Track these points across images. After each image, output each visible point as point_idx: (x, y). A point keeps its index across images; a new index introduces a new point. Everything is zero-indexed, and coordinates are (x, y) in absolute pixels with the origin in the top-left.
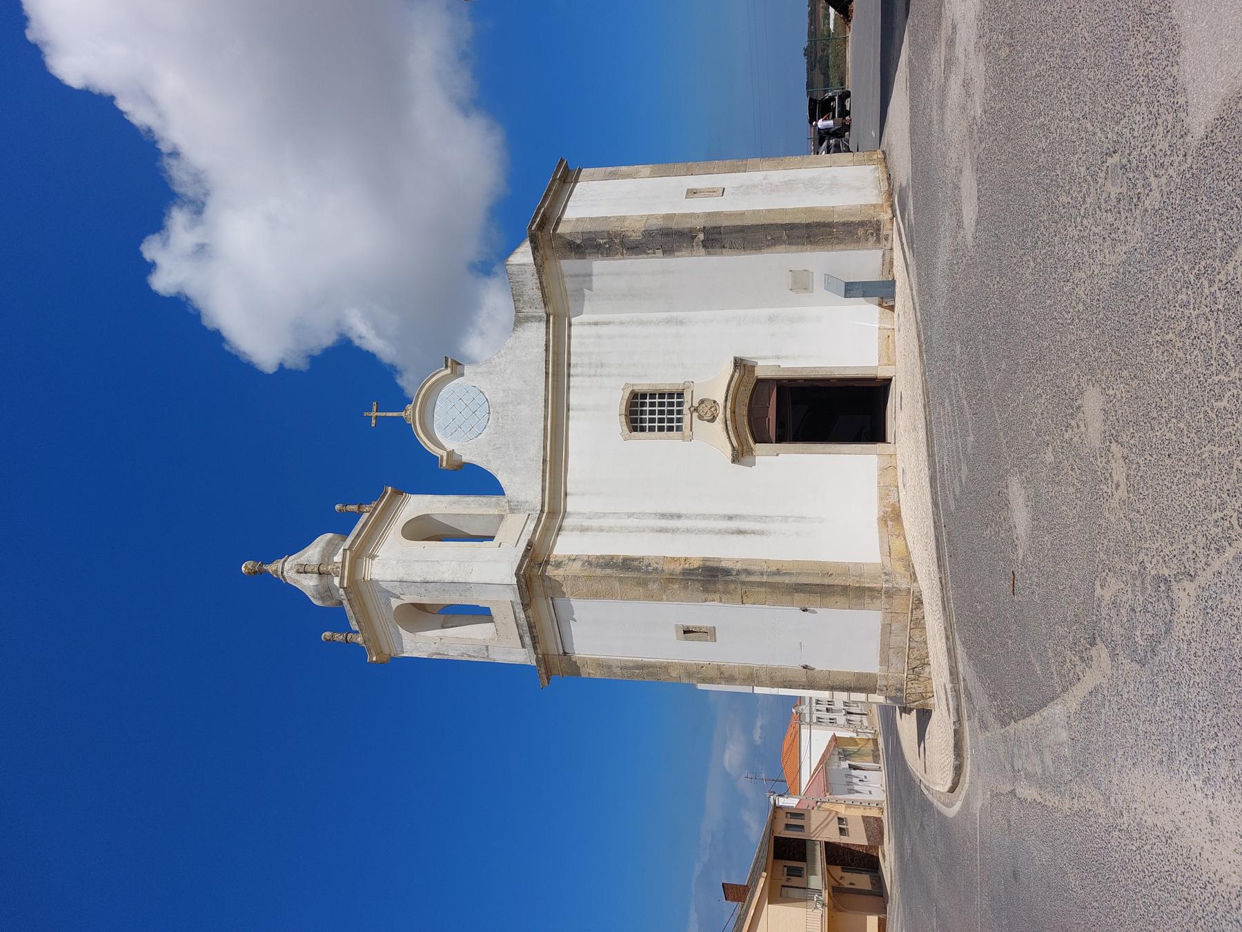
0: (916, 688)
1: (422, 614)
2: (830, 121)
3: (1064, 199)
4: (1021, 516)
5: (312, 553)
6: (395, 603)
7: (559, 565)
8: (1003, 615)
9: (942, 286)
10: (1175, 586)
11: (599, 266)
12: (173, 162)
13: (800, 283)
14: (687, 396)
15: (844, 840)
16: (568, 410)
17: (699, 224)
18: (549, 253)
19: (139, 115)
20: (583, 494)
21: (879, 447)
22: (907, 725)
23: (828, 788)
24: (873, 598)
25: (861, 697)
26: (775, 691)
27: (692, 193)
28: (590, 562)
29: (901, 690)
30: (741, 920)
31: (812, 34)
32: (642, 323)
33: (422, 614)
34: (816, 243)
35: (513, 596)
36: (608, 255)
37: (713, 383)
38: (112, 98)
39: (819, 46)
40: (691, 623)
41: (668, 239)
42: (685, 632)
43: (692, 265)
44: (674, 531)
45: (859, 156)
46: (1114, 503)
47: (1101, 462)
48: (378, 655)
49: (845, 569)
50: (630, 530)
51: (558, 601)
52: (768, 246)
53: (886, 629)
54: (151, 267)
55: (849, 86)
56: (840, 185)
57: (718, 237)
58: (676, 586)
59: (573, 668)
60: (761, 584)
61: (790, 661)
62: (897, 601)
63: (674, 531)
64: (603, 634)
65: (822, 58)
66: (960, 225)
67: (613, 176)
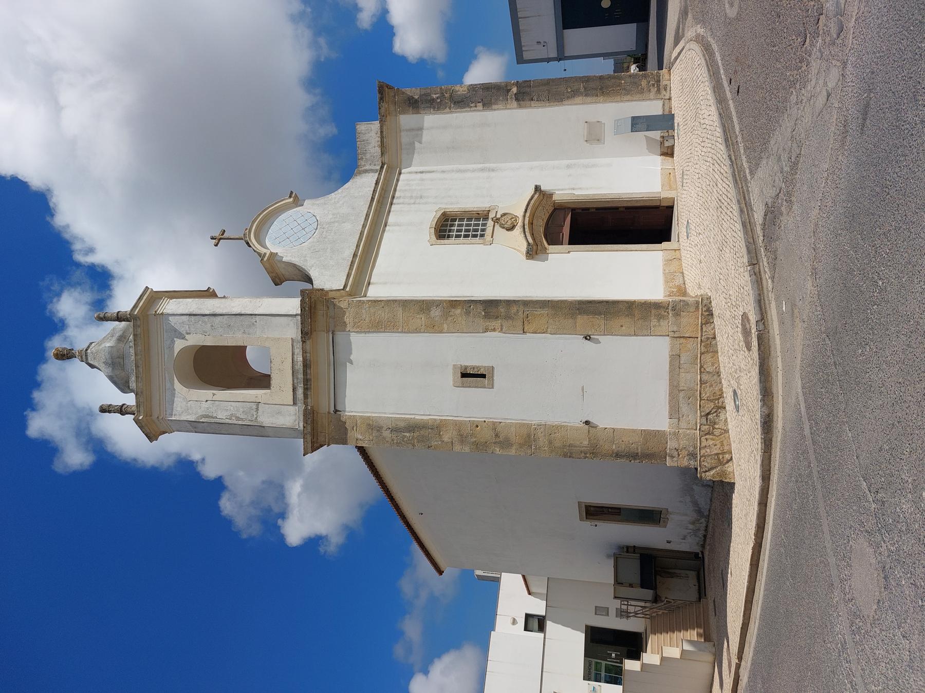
6: (179, 345)
11: (430, 120)
13: (594, 135)
16: (386, 225)
18: (392, 108)
20: (385, 283)
21: (665, 245)
24: (660, 317)
29: (693, 455)
32: (460, 171)
34: (608, 94)
36: (439, 109)
37: (515, 201)
40: (473, 361)
42: (464, 375)
48: (146, 416)
51: (340, 336)
52: (568, 98)
53: (675, 358)
58: (458, 311)
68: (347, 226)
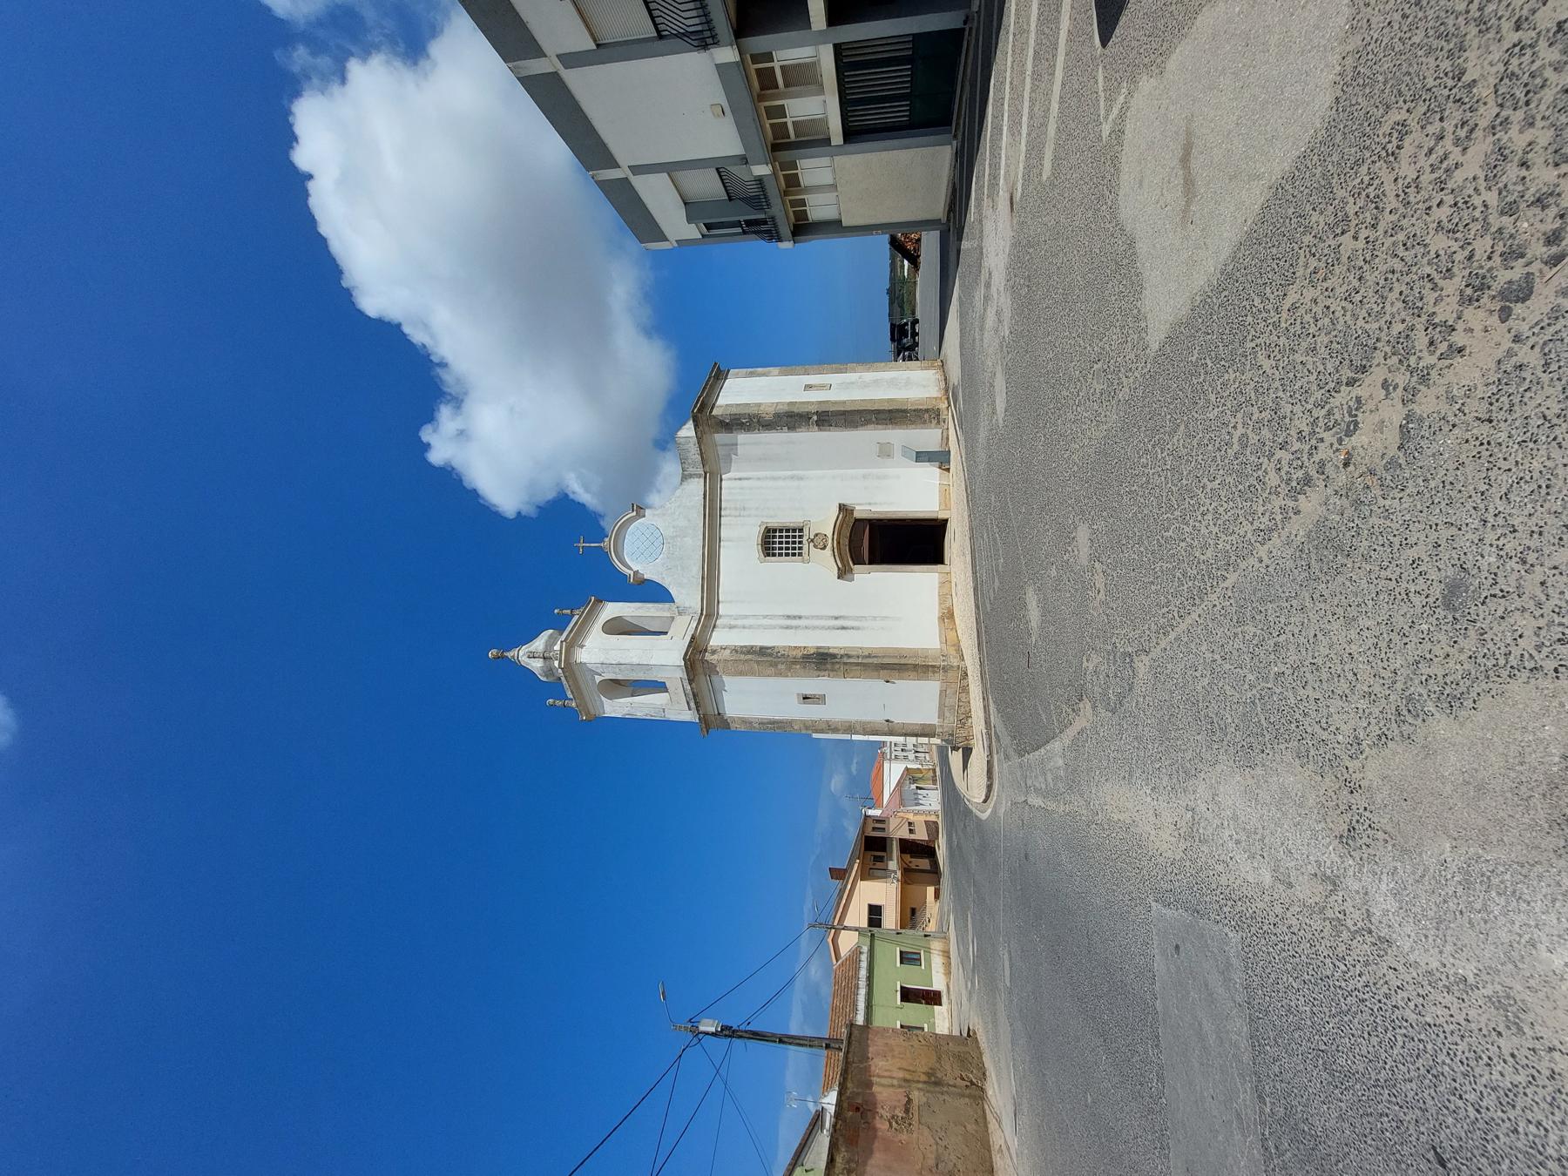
0: (963, 733)
1: (617, 687)
2: (904, 342)
3: (1065, 393)
4: (1034, 615)
5: (539, 644)
6: (598, 679)
7: (714, 652)
8: (1022, 680)
9: (982, 455)
10: (1136, 659)
11: (742, 438)
12: (439, 370)
13: (885, 452)
14: (806, 531)
15: (912, 837)
17: (813, 409)
19: (417, 336)
21: (939, 567)
22: (956, 758)
23: (902, 803)
25: (925, 740)
26: (866, 738)
27: (808, 387)
28: (735, 650)
30: (842, 891)
31: (892, 279)
32: (774, 478)
33: (617, 687)
35: (681, 674)
37: (825, 522)
38: (399, 326)
39: (898, 287)
40: (808, 692)
41: (792, 419)
43: (808, 439)
44: (797, 627)
45: (925, 363)
46: (1096, 603)
47: (1088, 575)
49: (915, 653)
50: (766, 627)
51: (714, 678)
53: (943, 693)
54: (427, 447)
55: (918, 316)
56: (912, 383)
57: (827, 418)
59: (724, 724)
60: (858, 664)
61: (876, 716)
62: (950, 674)
63: (797, 627)
64: (747, 700)
65: (900, 295)
66: (994, 409)
67: (751, 375)
68: (688, 540)
